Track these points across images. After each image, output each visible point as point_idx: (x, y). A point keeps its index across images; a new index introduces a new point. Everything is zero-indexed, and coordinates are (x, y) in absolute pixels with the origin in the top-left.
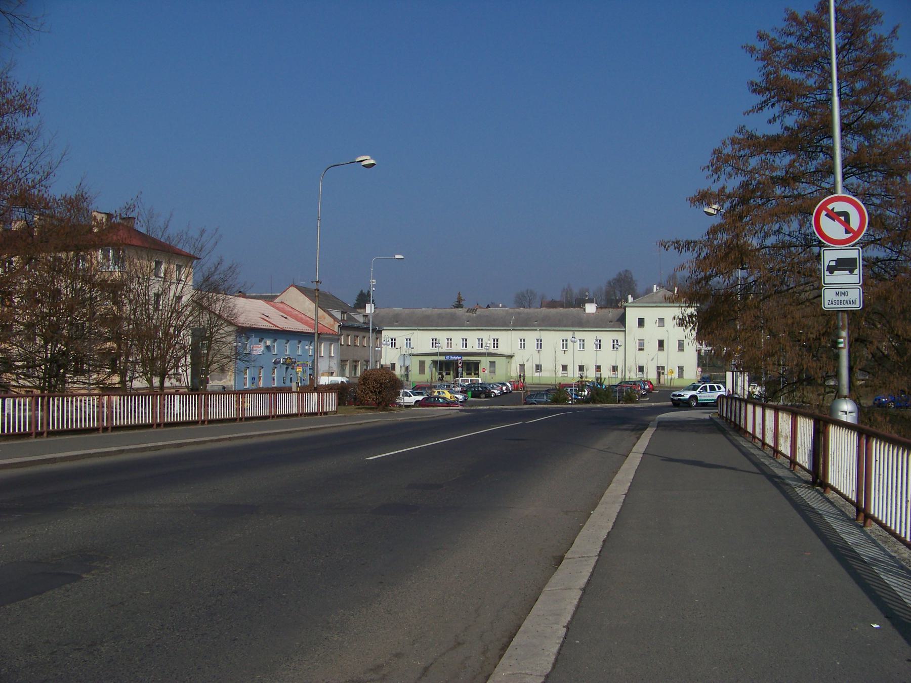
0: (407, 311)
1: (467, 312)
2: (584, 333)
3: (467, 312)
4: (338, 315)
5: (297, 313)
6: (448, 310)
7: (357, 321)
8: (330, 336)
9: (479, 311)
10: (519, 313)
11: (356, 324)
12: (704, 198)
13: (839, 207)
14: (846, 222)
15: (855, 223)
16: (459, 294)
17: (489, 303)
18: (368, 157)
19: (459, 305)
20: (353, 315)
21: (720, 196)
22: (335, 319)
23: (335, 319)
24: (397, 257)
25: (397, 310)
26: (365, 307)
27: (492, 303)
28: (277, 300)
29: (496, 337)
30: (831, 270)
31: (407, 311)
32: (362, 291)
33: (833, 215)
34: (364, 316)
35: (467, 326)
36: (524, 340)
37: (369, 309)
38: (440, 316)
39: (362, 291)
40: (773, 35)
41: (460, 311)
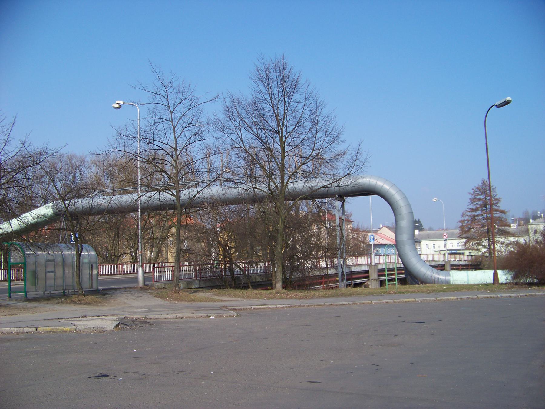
28: (379, 232)
40: (475, 189)
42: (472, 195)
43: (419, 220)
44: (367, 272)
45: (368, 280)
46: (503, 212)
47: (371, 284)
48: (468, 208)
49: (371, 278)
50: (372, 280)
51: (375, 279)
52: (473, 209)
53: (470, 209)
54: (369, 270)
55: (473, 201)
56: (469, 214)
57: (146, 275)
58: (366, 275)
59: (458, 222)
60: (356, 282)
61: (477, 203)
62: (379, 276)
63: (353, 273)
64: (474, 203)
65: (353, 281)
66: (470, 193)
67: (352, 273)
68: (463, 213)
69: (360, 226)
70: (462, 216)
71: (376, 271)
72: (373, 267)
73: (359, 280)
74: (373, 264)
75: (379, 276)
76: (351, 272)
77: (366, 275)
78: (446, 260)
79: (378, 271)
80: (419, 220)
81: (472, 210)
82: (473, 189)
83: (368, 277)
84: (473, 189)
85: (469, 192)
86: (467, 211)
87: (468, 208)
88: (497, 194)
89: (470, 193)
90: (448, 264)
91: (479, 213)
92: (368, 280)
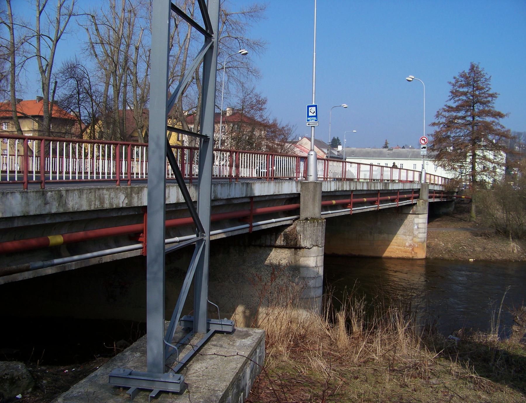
0: (358, 149)
1: (388, 150)
2: (416, 161)
3: (388, 150)
4: (326, 151)
5: (307, 150)
6: (379, 150)
7: (334, 154)
8: (332, 159)
9: (394, 150)
10: (414, 152)
11: (334, 156)
12: (434, 124)
13: (424, 138)
14: (425, 141)
15: (426, 141)
16: (386, 140)
17: (404, 145)
18: (345, 105)
19: (386, 147)
20: (333, 151)
21: (439, 124)
22: (325, 153)
23: (325, 153)
24: (354, 131)
25: (354, 149)
26: (337, 147)
27: (406, 145)
28: (298, 144)
29: (402, 163)
30: (422, 148)
31: (358, 149)
32: (334, 137)
33: (423, 140)
34: (338, 151)
35: (388, 158)
36: (416, 165)
37: (340, 148)
38: (374, 152)
39: (334, 137)
40: (457, 77)
41: (385, 150)
42: (454, 85)
43: (338, 138)
44: (295, 198)
45: (296, 219)
46: (499, 115)
47: (304, 230)
48: (445, 106)
49: (303, 216)
50: (307, 219)
51: (313, 219)
52: (452, 108)
53: (449, 107)
54: (299, 194)
55: (455, 94)
56: (447, 114)
57: (213, 180)
58: (292, 206)
59: (429, 125)
60: (264, 227)
61: (461, 97)
62: (324, 208)
63: (258, 199)
64: (457, 99)
65: (254, 224)
66: (450, 83)
67: (254, 200)
68: (438, 112)
69: (278, 122)
70: (437, 116)
71: (318, 197)
72: (311, 187)
73: (274, 220)
74: (311, 179)
75: (324, 208)
76: (252, 198)
77: (292, 206)
78: (423, 182)
79: (322, 196)
80: (338, 138)
81: (450, 109)
82: (454, 78)
83: (296, 212)
84: (454, 78)
85: (450, 81)
86: (444, 109)
87: (445, 106)
88: (490, 89)
89: (450, 83)
90: (425, 188)
91: (461, 114)
92: (296, 219)
